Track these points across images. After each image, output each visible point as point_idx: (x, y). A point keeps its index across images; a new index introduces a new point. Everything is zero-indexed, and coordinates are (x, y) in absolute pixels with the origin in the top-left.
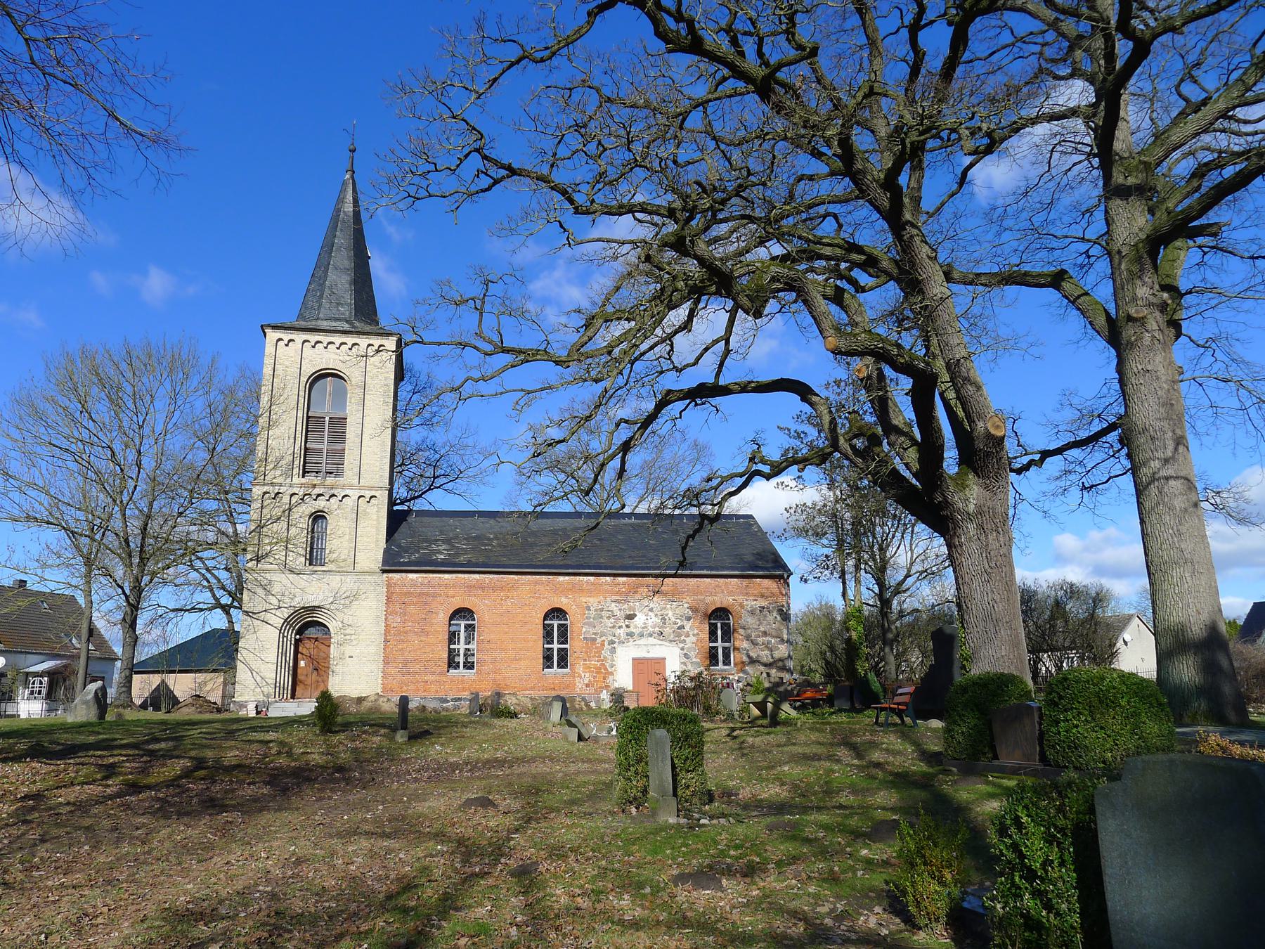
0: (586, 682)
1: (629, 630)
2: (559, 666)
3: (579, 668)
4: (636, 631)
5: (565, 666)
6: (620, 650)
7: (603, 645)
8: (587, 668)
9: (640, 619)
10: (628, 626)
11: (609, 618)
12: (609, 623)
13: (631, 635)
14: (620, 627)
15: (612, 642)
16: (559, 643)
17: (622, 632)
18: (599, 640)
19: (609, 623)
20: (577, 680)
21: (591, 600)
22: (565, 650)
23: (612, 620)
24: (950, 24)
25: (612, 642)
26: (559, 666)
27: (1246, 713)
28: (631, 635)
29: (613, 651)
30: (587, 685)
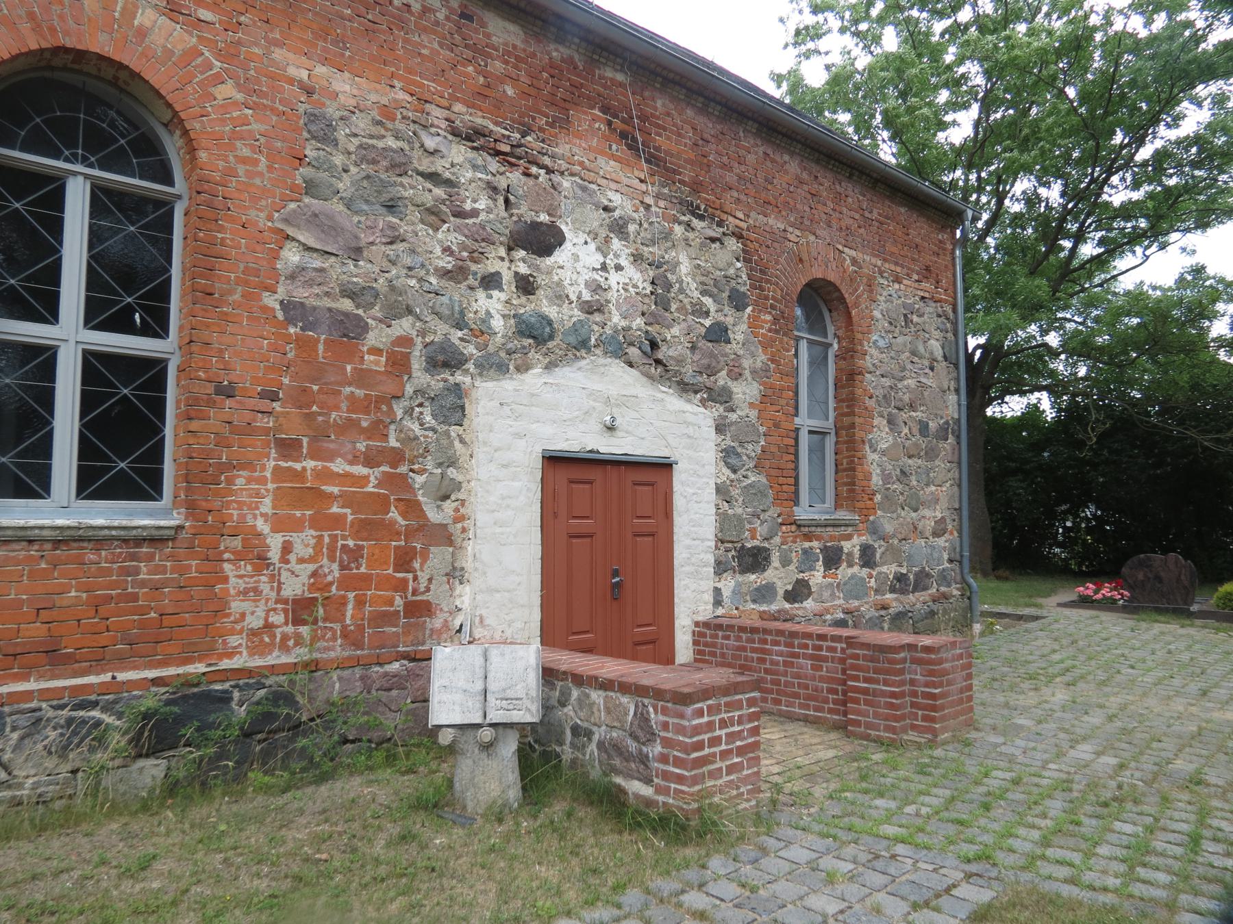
0: (294, 586)
1: (527, 307)
2: (91, 484)
3: (255, 501)
4: (564, 315)
5: (143, 484)
6: (489, 398)
7: (399, 364)
8: (302, 497)
9: (576, 261)
10: (526, 286)
11: (434, 216)
12: (438, 244)
13: (535, 333)
14: (490, 282)
15: (445, 360)
16: (100, 314)
17: (493, 307)
18: (378, 336)
19: (438, 244)
20: (235, 576)
21: (344, 85)
22: (150, 374)
23: (449, 235)
24: (828, 67)
25: (445, 360)
26: (91, 484)
27: (1107, 204)
28: (535, 333)
29: (453, 408)
30: (300, 610)
